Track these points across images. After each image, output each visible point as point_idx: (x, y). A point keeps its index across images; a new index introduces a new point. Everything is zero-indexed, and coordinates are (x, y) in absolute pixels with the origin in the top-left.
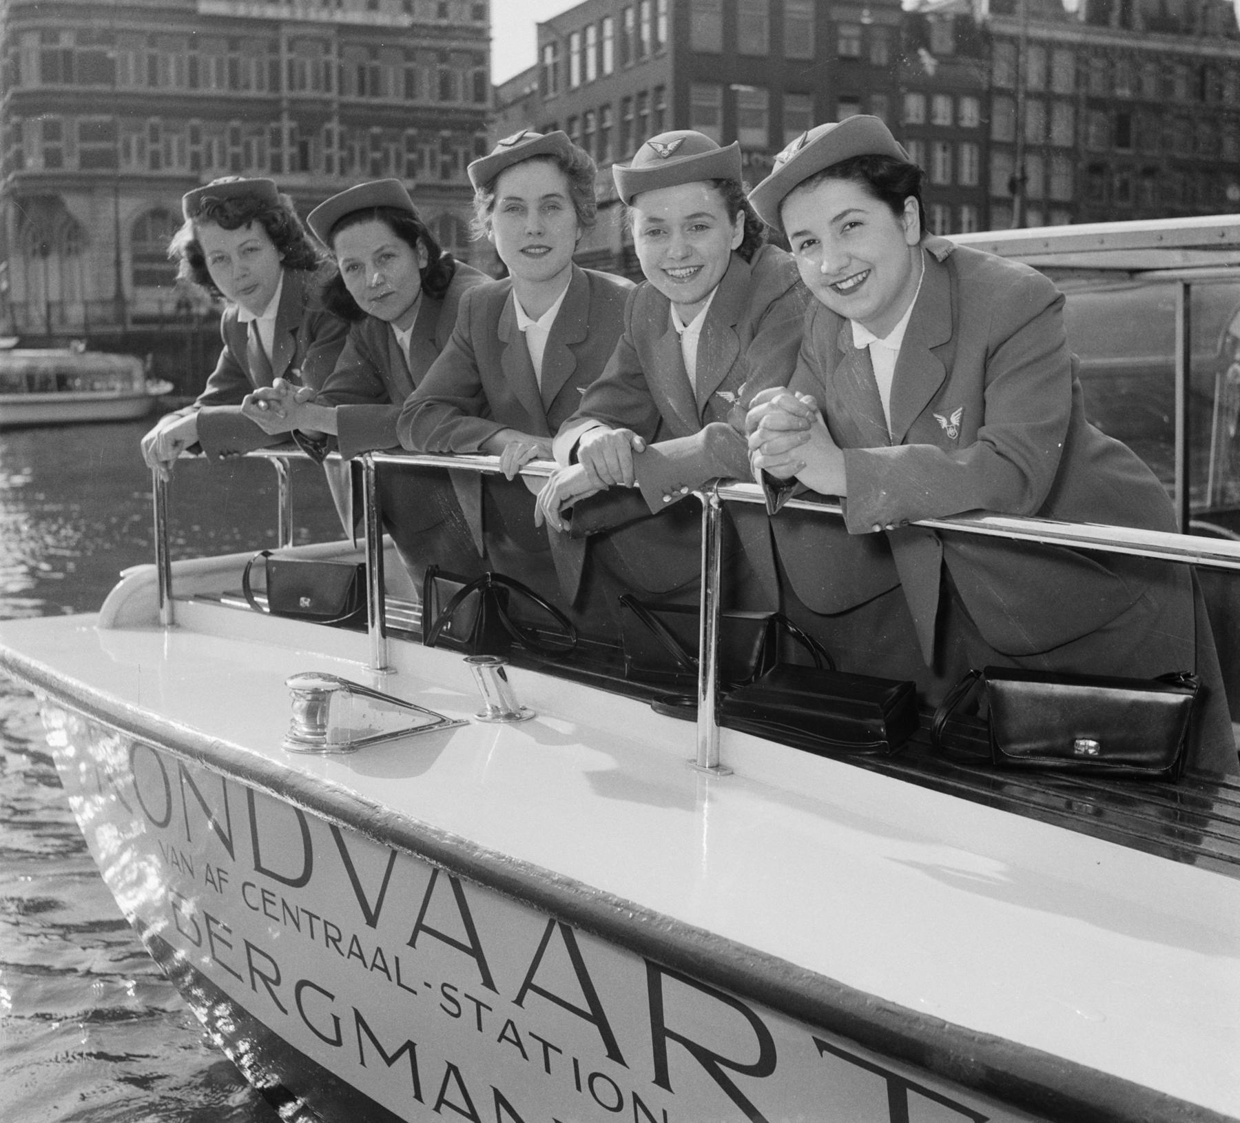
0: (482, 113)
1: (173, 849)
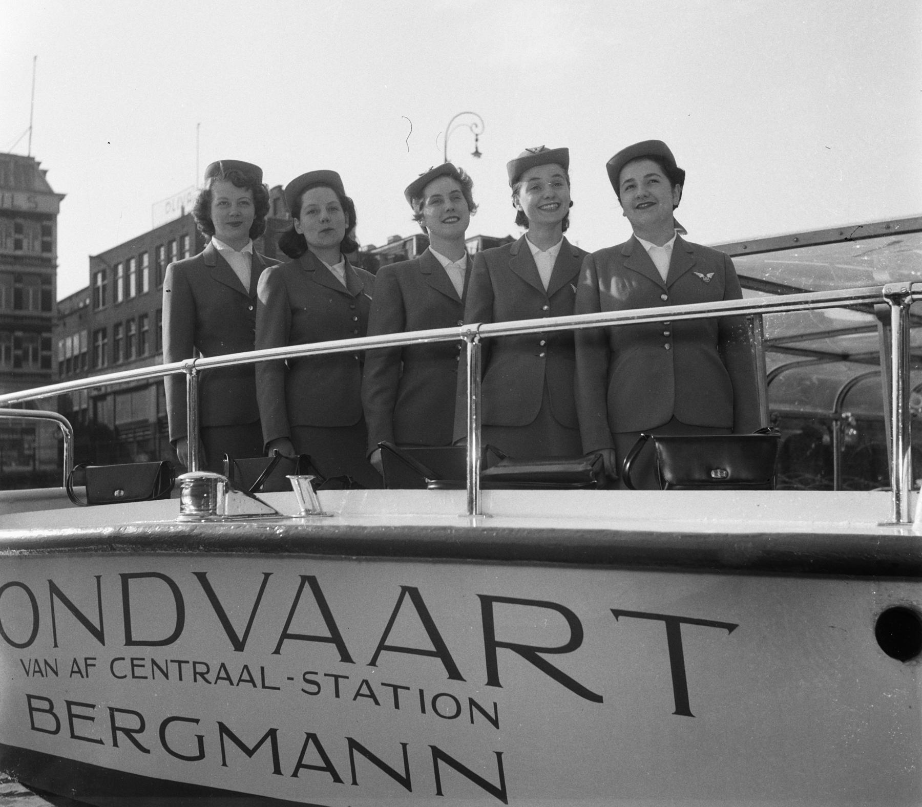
0: (49, 319)
1: (36, 661)
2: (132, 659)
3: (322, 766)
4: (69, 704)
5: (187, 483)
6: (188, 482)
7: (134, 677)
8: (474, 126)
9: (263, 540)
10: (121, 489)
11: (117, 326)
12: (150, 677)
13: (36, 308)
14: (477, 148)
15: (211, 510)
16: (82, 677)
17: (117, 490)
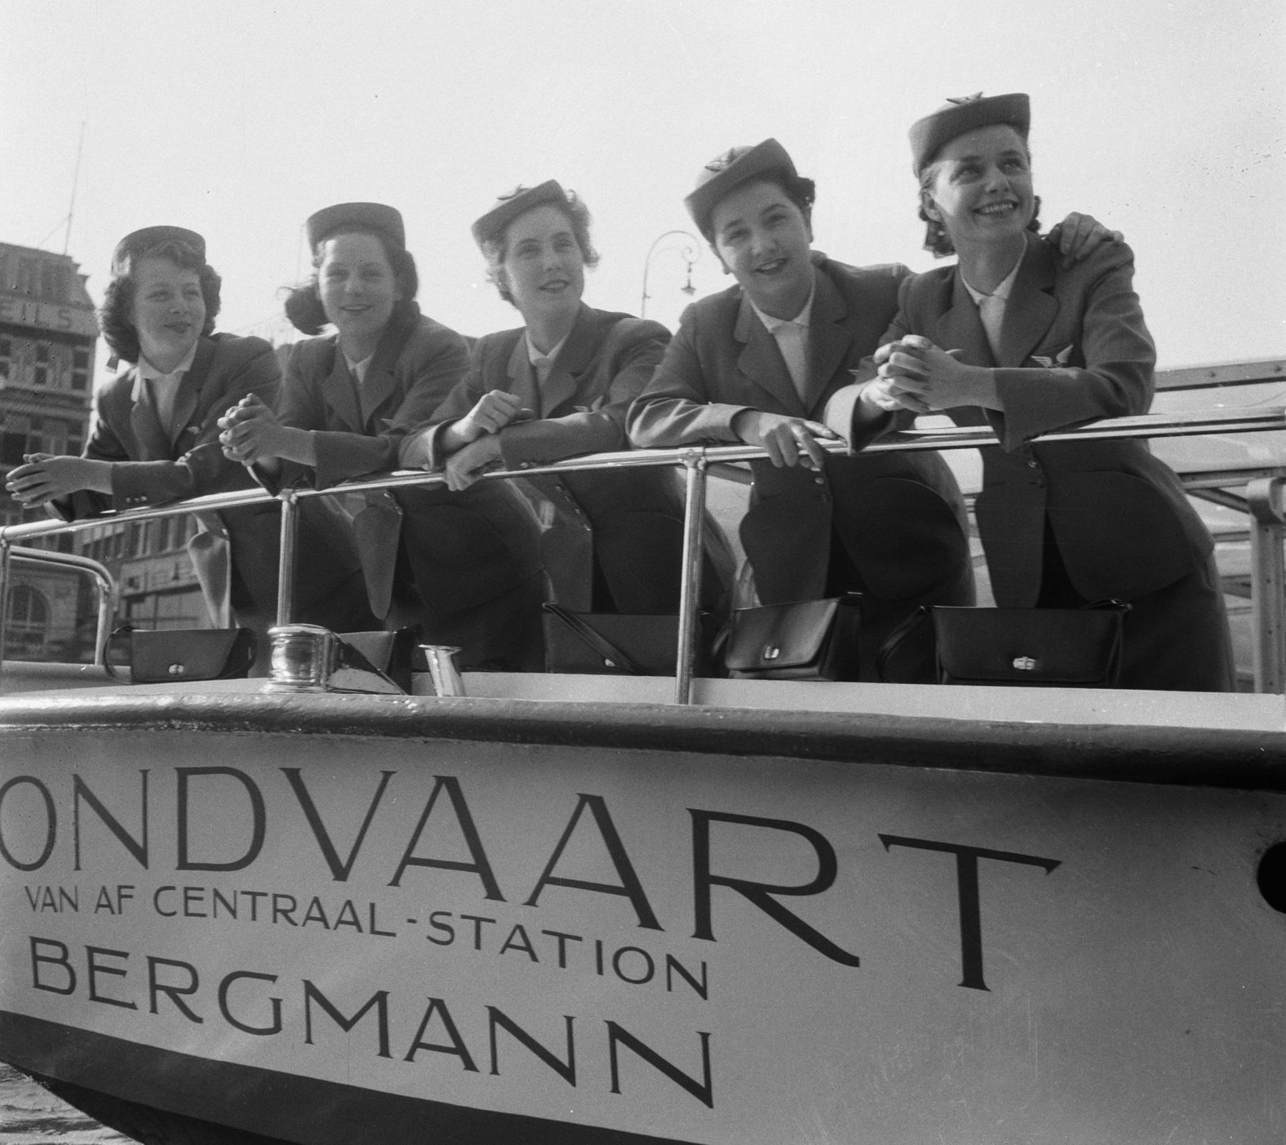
1: (48, 889)
2: (187, 889)
3: (450, 1046)
4: (91, 951)
5: (282, 639)
6: (283, 637)
7: (187, 914)
8: (688, 251)
9: (386, 718)
10: (179, 664)
12: (210, 913)
14: (689, 281)
15: (312, 678)
16: (113, 913)
17: (173, 664)
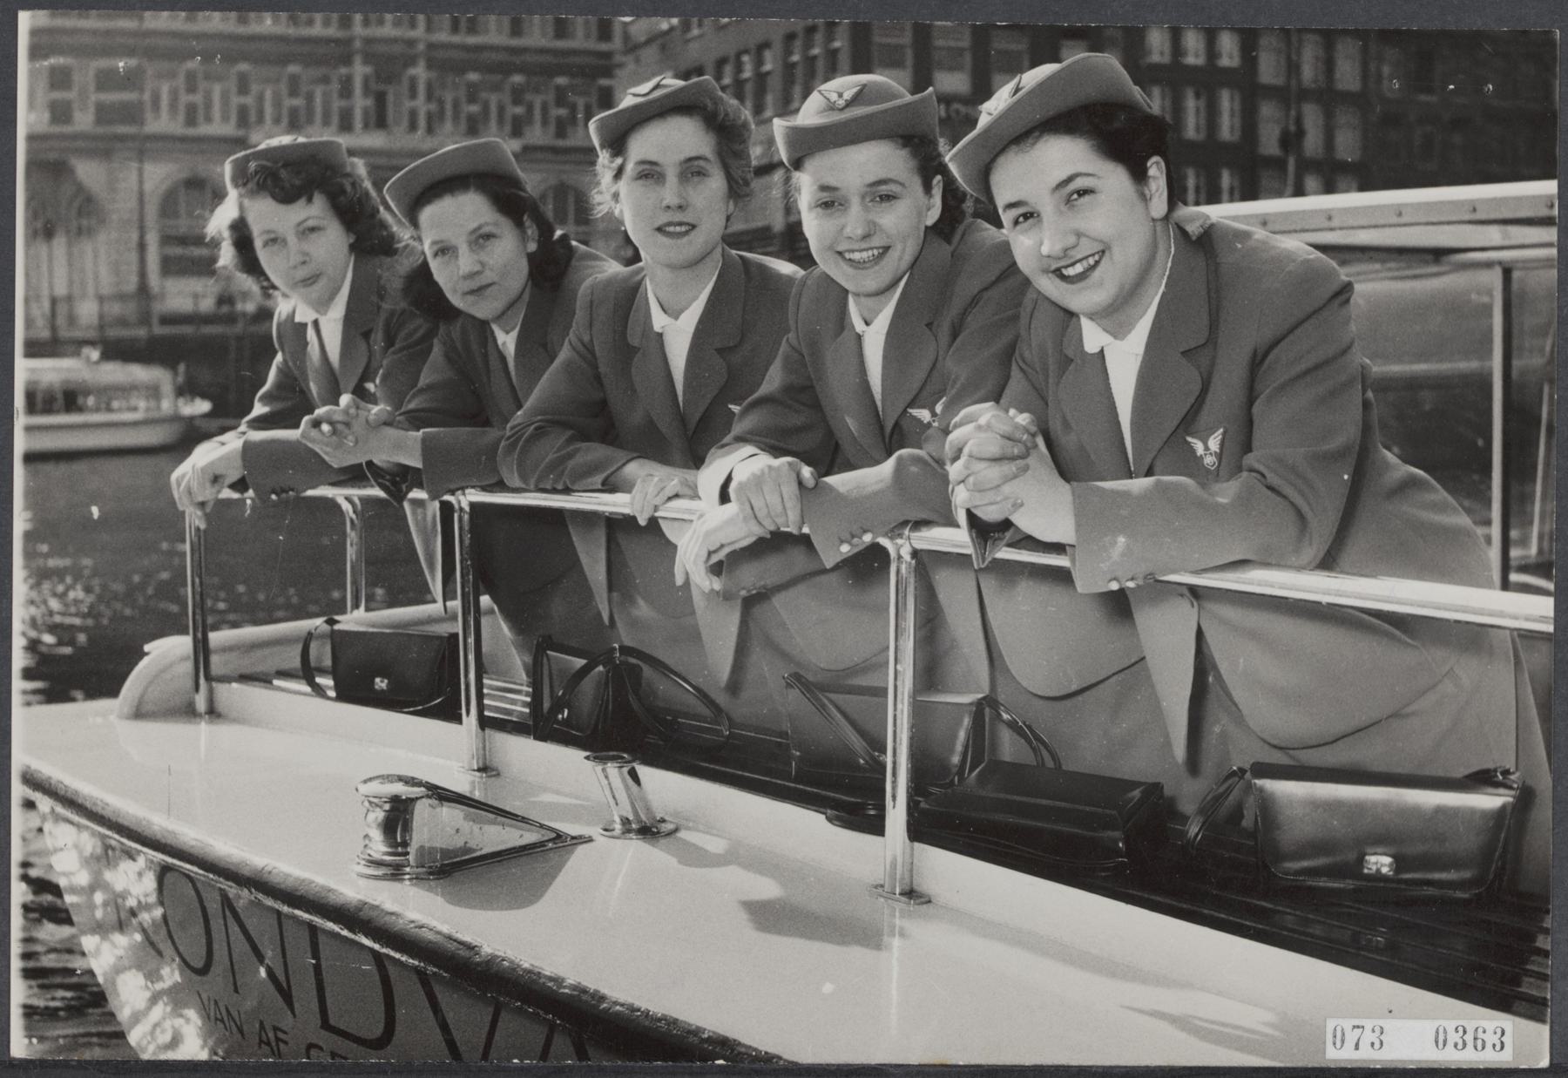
0: (608, 55)
11: (721, 63)
13: (587, 36)
